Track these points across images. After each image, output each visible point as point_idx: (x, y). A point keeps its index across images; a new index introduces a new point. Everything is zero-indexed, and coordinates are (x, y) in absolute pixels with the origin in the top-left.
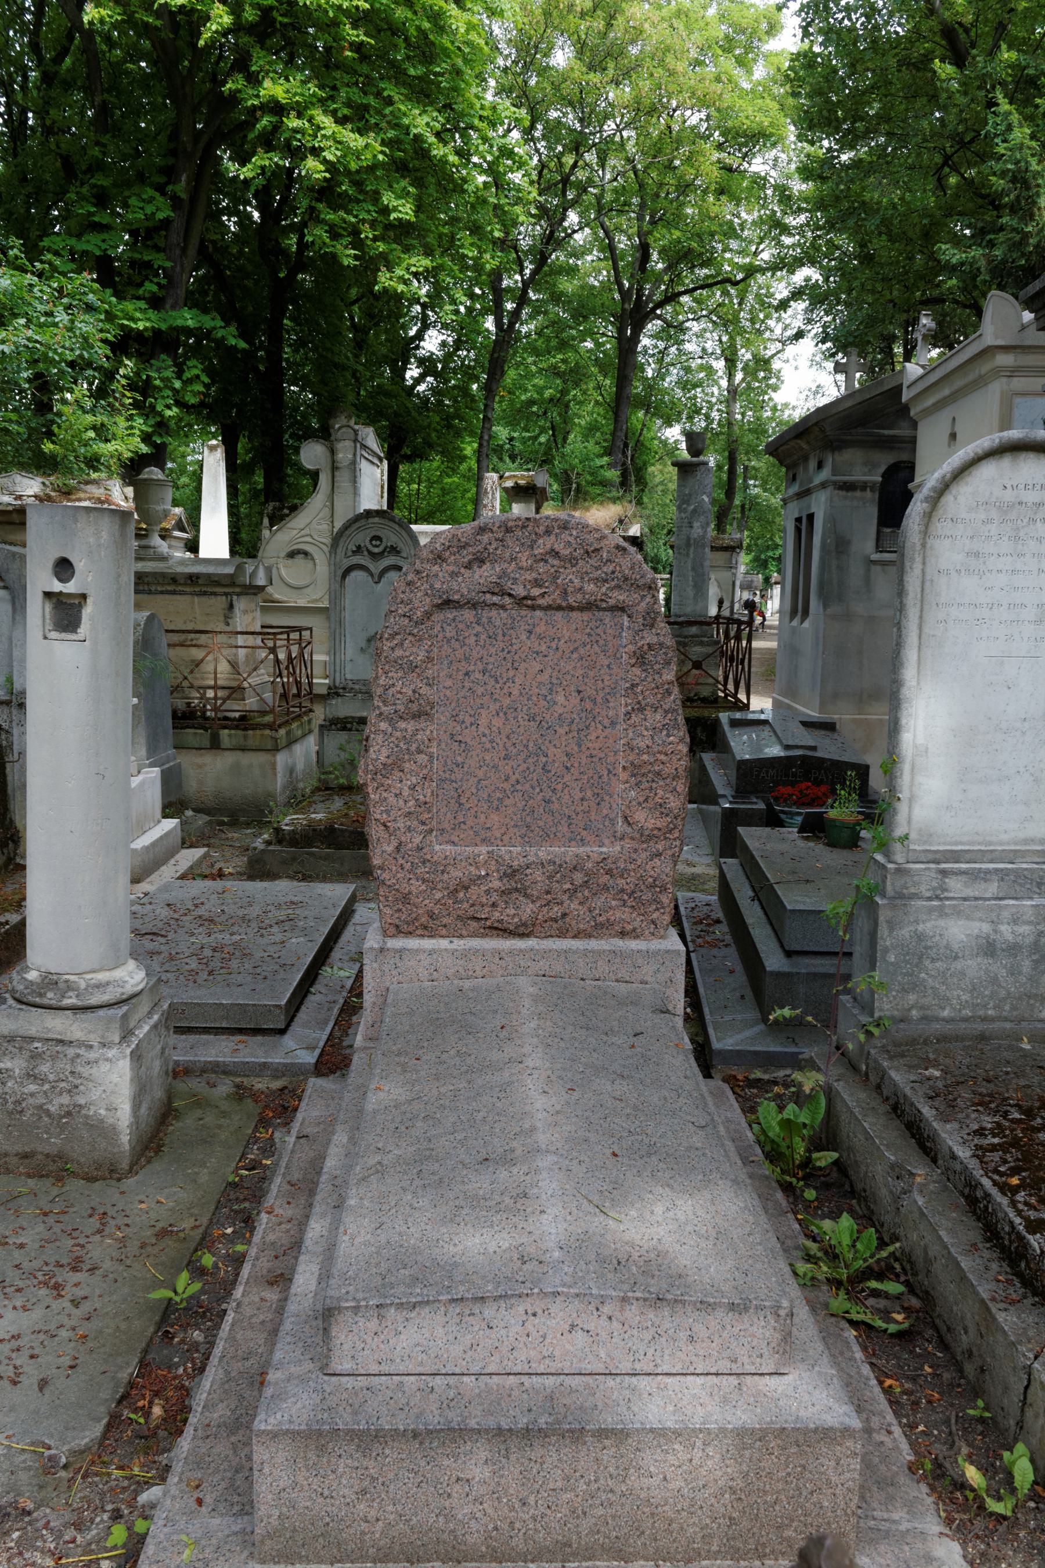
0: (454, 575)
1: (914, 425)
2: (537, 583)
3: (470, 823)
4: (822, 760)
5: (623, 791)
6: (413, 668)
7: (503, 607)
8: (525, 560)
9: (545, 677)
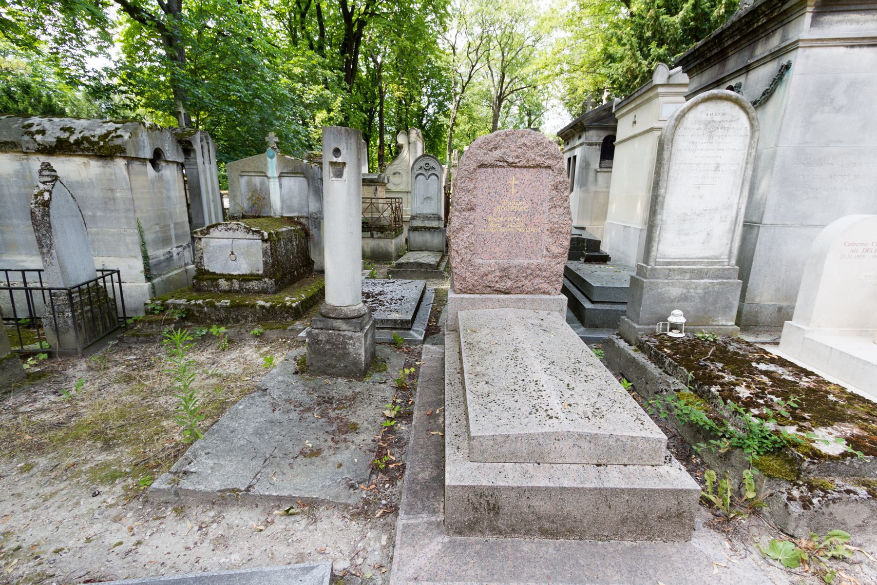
0: (485, 154)
1: (616, 121)
2: (517, 157)
3: (489, 250)
4: (584, 239)
5: (546, 237)
6: (469, 191)
7: (503, 167)
8: (513, 147)
9: (519, 194)
